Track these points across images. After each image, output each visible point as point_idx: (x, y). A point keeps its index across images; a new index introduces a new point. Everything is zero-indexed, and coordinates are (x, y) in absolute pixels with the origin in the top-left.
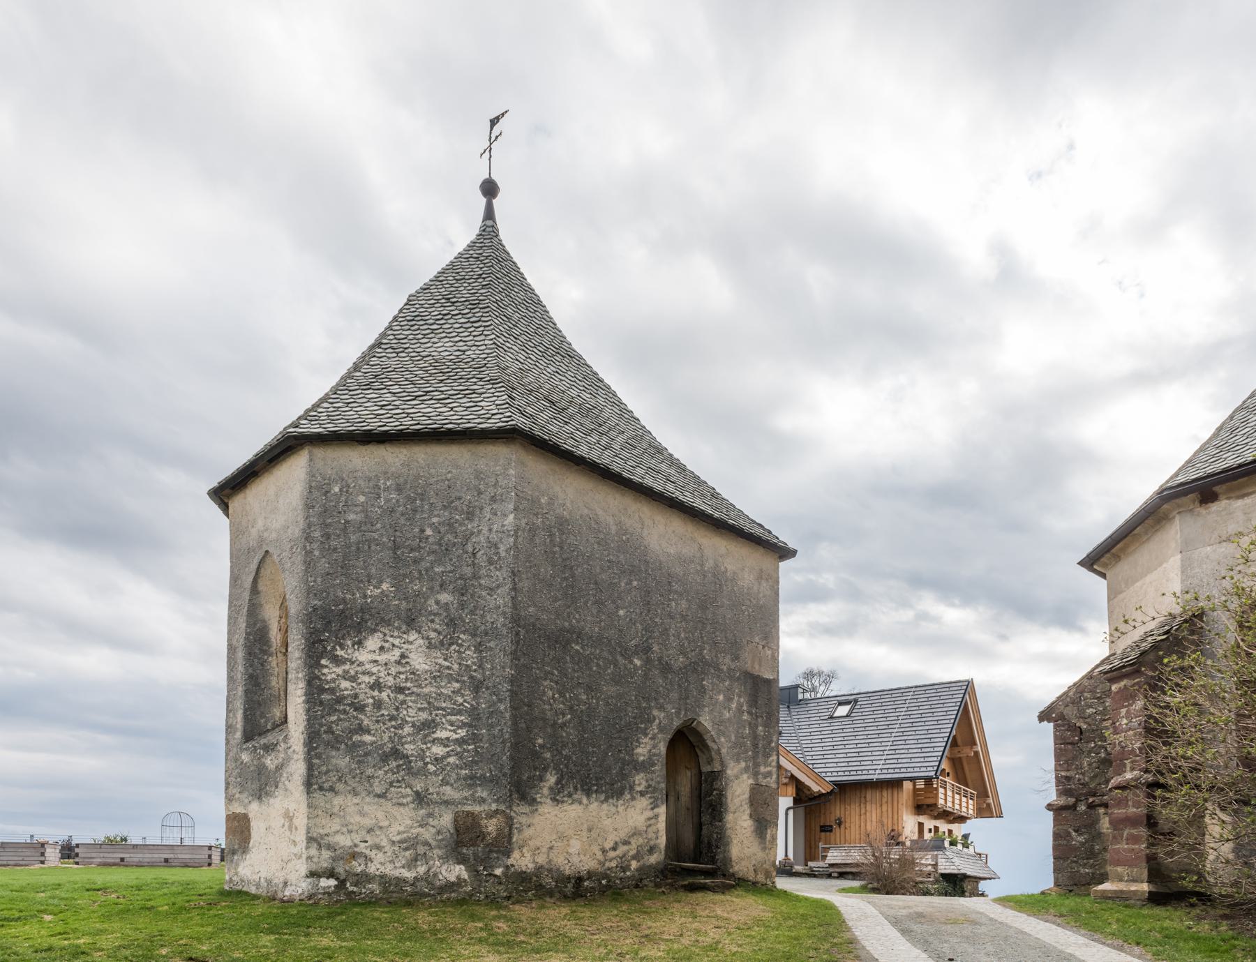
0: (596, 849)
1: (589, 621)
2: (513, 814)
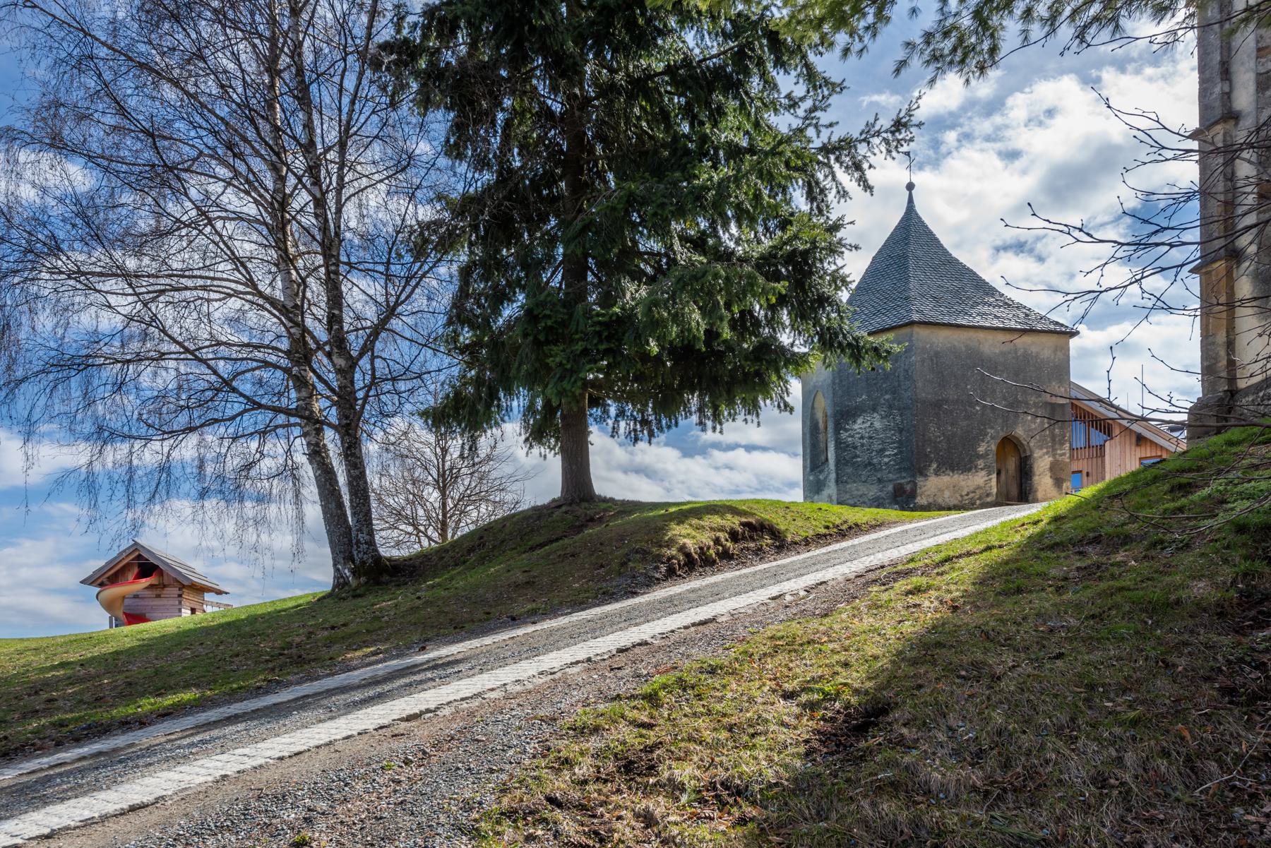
0: (958, 495)
1: (952, 394)
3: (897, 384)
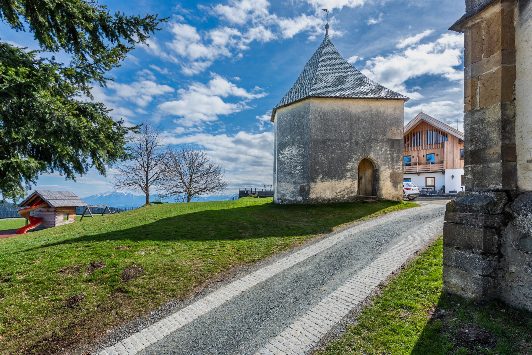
3: (302, 130)
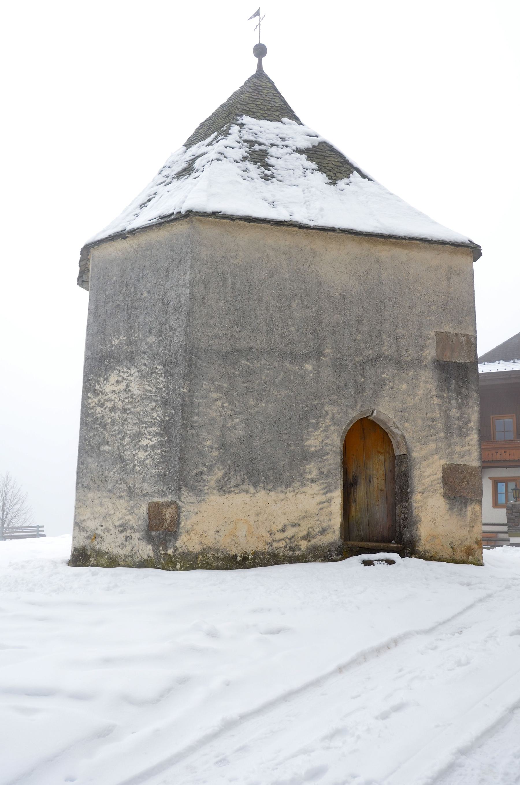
2: (180, 504)
